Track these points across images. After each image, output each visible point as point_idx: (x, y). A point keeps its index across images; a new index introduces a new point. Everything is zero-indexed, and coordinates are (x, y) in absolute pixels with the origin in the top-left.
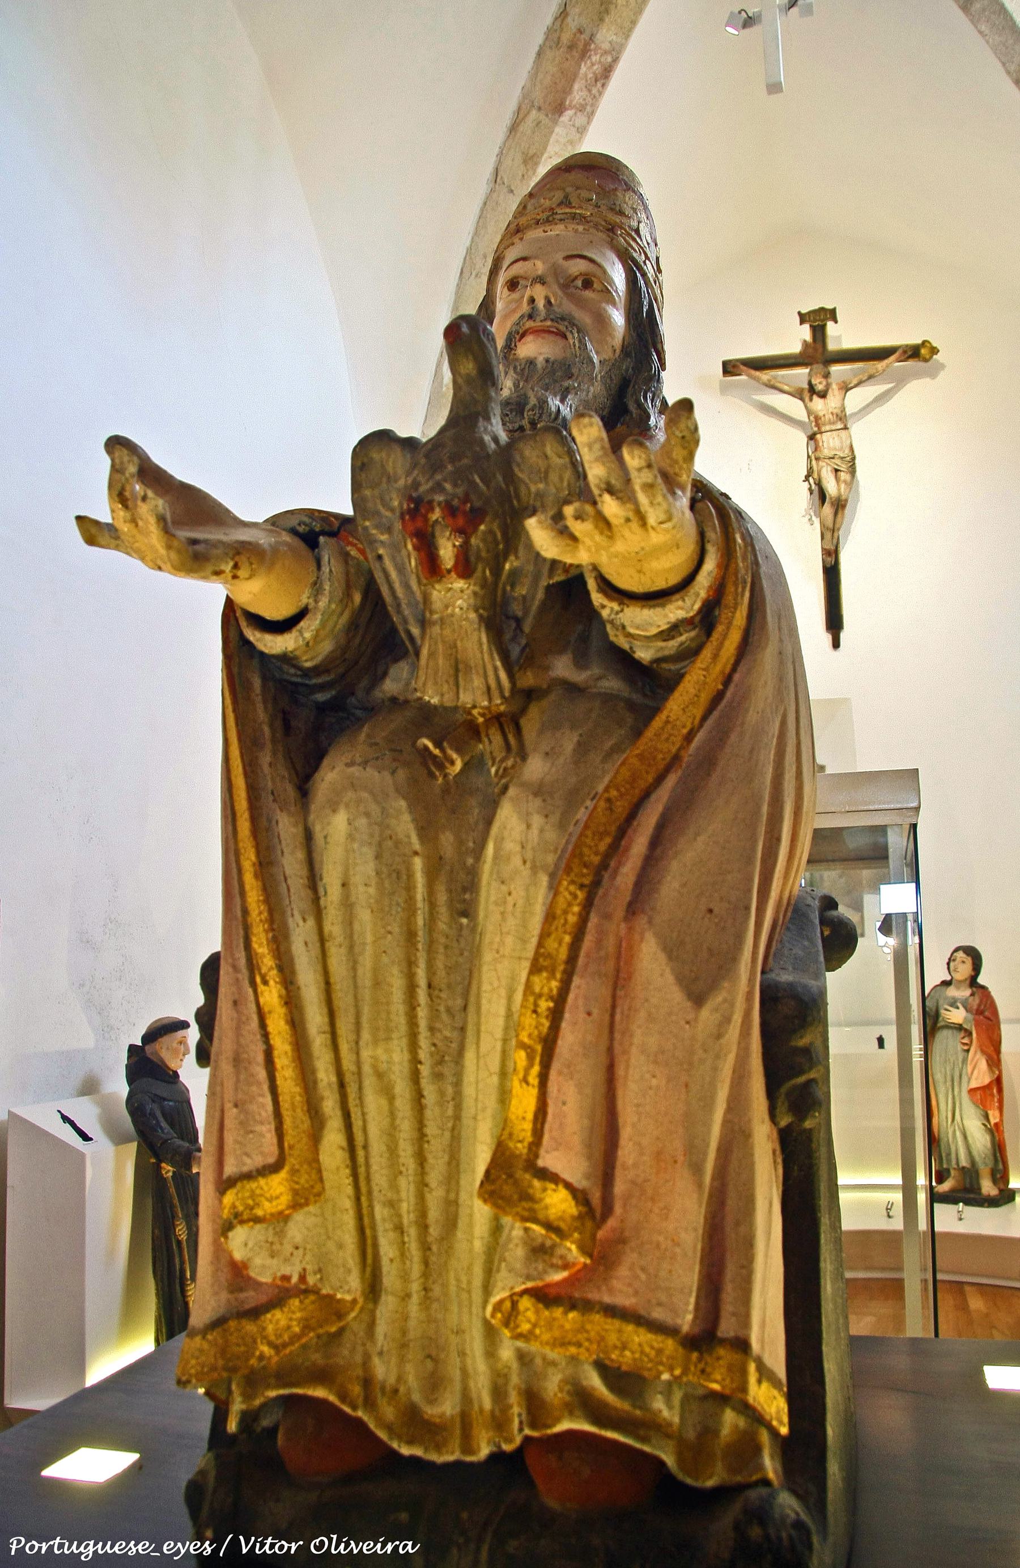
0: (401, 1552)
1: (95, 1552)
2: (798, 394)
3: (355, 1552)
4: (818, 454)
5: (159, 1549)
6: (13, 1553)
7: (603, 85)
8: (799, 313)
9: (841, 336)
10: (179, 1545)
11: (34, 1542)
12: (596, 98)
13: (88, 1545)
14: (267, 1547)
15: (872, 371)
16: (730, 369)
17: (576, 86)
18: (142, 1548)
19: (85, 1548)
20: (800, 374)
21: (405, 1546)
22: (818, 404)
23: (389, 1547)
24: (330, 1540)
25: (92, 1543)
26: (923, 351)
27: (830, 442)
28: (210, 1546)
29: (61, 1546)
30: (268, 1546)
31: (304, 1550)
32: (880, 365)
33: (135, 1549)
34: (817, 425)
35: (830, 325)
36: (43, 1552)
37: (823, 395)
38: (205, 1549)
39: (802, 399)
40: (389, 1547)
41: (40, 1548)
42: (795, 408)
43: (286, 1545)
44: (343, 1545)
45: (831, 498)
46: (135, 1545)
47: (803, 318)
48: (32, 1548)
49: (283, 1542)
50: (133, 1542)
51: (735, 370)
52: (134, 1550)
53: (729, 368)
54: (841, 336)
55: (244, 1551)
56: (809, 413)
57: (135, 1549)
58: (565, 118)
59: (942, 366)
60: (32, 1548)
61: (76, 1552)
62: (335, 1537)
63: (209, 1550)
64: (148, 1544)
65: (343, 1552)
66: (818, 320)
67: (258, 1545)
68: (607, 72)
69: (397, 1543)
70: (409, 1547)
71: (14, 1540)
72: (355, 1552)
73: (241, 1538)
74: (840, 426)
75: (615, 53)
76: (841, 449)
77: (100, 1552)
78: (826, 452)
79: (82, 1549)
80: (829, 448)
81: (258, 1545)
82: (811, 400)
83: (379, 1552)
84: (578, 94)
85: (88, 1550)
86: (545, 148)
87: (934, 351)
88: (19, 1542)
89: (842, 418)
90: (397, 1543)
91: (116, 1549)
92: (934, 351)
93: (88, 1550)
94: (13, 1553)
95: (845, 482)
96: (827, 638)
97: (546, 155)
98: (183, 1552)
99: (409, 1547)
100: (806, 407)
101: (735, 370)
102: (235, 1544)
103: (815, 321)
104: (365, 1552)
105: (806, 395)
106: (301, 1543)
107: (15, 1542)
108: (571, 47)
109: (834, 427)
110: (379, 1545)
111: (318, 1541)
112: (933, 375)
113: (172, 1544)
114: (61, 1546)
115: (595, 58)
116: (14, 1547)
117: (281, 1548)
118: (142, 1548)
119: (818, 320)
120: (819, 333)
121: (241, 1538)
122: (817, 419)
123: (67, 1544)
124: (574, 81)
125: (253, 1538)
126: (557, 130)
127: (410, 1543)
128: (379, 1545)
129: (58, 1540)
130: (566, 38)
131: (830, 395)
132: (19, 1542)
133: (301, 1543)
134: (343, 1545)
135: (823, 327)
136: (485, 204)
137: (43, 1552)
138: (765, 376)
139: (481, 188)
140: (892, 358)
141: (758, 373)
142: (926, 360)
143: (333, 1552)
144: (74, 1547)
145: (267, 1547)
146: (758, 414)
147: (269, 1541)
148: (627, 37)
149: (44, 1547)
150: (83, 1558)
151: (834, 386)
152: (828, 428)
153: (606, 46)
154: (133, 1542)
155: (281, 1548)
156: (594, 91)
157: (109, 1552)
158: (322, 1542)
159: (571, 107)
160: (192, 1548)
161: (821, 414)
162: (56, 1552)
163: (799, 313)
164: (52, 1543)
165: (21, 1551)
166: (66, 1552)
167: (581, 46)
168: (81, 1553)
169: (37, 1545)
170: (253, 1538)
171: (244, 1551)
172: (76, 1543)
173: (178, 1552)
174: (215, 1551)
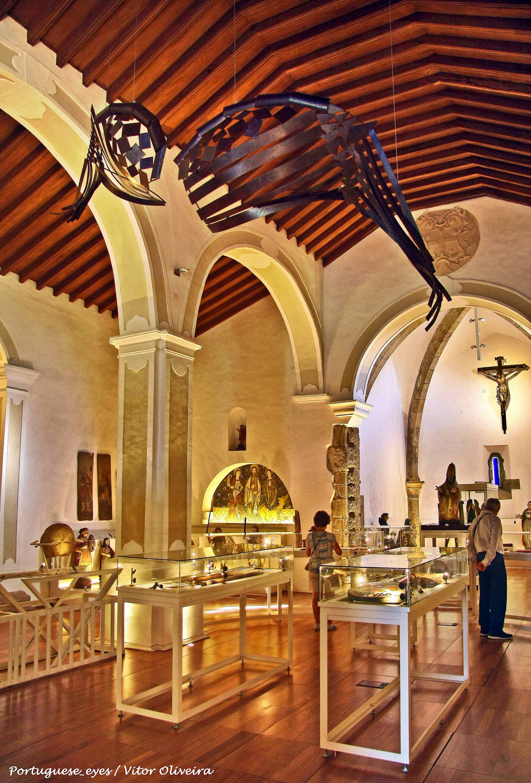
0: (205, 774)
1: (52, 774)
3: (182, 774)
5: (84, 772)
6: (11, 774)
10: (94, 770)
11: (21, 769)
13: (48, 770)
14: (138, 772)
18: (75, 772)
21: (207, 771)
24: (169, 768)
25: (50, 769)
28: (109, 771)
29: (35, 771)
30: (139, 771)
31: (156, 773)
36: (26, 774)
40: (199, 772)
44: (176, 770)
46: (72, 771)
48: (21, 772)
50: (71, 769)
55: (127, 773)
60: (21, 772)
61: (42, 774)
62: (172, 766)
63: (109, 773)
67: (133, 770)
69: (203, 769)
70: (209, 772)
71: (12, 768)
72: (182, 774)
73: (125, 767)
77: (54, 774)
79: (45, 772)
81: (133, 770)
83: (194, 774)
84: (445, 339)
85: (49, 773)
90: (203, 769)
91: (62, 772)
94: (11, 774)
98: (96, 774)
99: (209, 772)
106: (155, 769)
107: (12, 769)
110: (194, 771)
111: (163, 768)
114: (35, 771)
116: (12, 771)
117: (145, 772)
121: (125, 767)
123: (38, 770)
125: (131, 767)
127: (209, 770)
128: (194, 771)
130: (442, 330)
133: (155, 769)
134: (176, 770)
145: (138, 772)
147: (139, 768)
154: (71, 769)
155: (145, 772)
157: (59, 774)
158: (165, 769)
164: (30, 769)
165: (15, 773)
166: (38, 774)
168: (45, 775)
169: (23, 771)
170: (131, 767)
171: (127, 773)
173: (94, 774)
174: (112, 774)
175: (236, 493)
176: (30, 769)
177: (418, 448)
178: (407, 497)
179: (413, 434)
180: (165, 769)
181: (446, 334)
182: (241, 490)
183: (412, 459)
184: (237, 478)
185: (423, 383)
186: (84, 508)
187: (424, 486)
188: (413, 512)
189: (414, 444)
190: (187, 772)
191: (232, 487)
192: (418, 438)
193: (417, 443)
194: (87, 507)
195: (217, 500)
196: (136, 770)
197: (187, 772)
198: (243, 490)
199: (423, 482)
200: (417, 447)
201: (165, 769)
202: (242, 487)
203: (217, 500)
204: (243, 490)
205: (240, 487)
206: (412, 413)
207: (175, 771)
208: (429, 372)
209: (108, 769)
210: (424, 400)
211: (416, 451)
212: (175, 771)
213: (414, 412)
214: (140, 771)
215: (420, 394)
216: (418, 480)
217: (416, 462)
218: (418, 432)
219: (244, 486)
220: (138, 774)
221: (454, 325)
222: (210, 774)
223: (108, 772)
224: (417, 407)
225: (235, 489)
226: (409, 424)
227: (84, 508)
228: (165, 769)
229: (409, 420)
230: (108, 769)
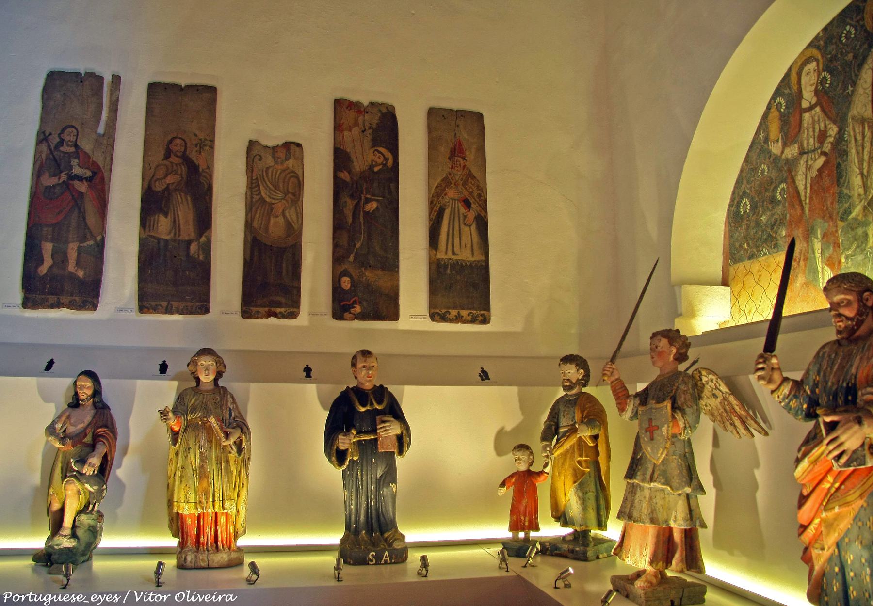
5: (88, 599)
23: (220, 598)
29: (33, 597)
40: (220, 598)
91: (64, 599)
114: (33, 597)
116: (6, 598)
129: (31, 594)
132: (9, 595)
138: (597, 479)
147: (151, 594)
158: (181, 595)
165: (10, 600)
174: (121, 600)
175: (808, 168)
180: (181, 595)
182: (827, 147)
184: (808, 97)
186: (48, 262)
191: (792, 151)
194: (65, 260)
195: (741, 232)
196: (148, 597)
198: (840, 138)
202: (833, 130)
203: (741, 232)
204: (840, 138)
205: (822, 136)
207: (193, 597)
212: (193, 597)
214: (153, 597)
219: (841, 121)
225: (802, 152)
227: (48, 262)
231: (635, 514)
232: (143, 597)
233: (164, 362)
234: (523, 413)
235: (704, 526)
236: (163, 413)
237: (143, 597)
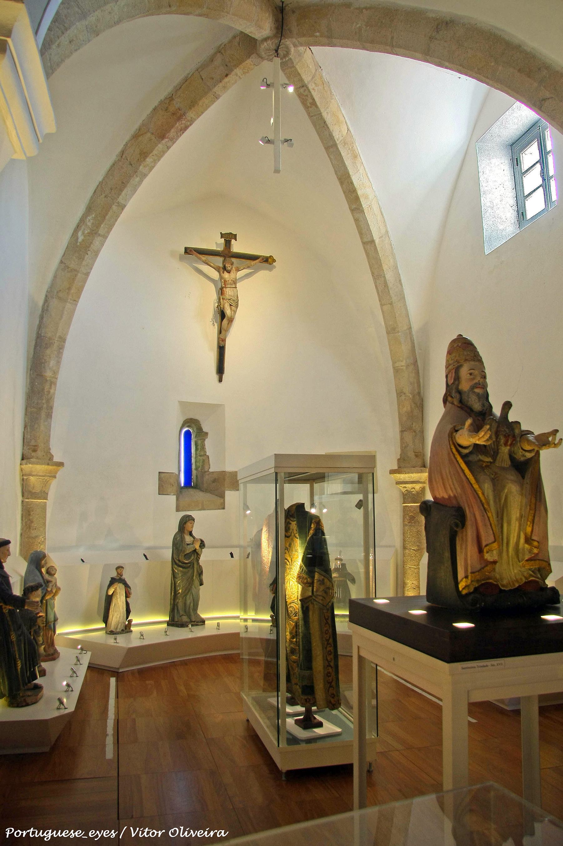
0: (218, 836)
1: (52, 836)
2: (217, 269)
3: (193, 836)
4: (224, 297)
6: (7, 837)
7: (183, 133)
8: (221, 233)
9: (237, 247)
10: (98, 832)
11: (19, 831)
12: (178, 137)
13: (48, 832)
14: (145, 833)
15: (249, 265)
16: (188, 251)
17: (173, 130)
18: (77, 834)
19: (47, 834)
20: (219, 261)
21: (221, 832)
22: (226, 275)
23: (212, 833)
24: (180, 830)
25: (50, 831)
26: (269, 260)
27: (229, 292)
28: (115, 833)
29: (34, 833)
30: (146, 833)
31: (165, 835)
32: (253, 263)
33: (73, 834)
34: (225, 284)
35: (233, 241)
36: (24, 836)
37: (229, 272)
38: (112, 834)
39: (219, 272)
40: (212, 833)
41: (22, 834)
42: (215, 275)
43: (156, 832)
44: (186, 832)
45: (228, 317)
46: (74, 832)
47: (222, 235)
48: (18, 834)
49: (154, 831)
50: (73, 831)
51: (191, 253)
52: (73, 835)
53: (188, 251)
54: (237, 247)
55: (133, 835)
56: (221, 277)
57: (73, 834)
58: (164, 142)
59: (275, 267)
60: (18, 834)
61: (42, 836)
62: (182, 828)
63: (114, 835)
64: (81, 832)
65: (186, 836)
66: (229, 238)
67: (140, 832)
68: (186, 128)
69: (216, 831)
70: (223, 833)
71: (8, 830)
72: (193, 836)
73: (131, 828)
74: (234, 286)
75: (192, 122)
76: (234, 296)
77: (55, 836)
78: (227, 297)
79: (45, 834)
80: (229, 295)
81: (140, 832)
82: (223, 273)
83: (206, 836)
84: (172, 133)
85: (48, 835)
86: (152, 151)
87: (274, 261)
88: (11, 831)
89: (235, 282)
90: (216, 831)
91: (63, 834)
92: (274, 261)
93: (48, 835)
94: (7, 837)
95: (234, 311)
96: (216, 377)
97: (151, 154)
98: (100, 836)
99: (223, 833)
100: (220, 275)
101: (191, 253)
102: (128, 832)
103: (227, 238)
104: (105, 836)
105: (222, 271)
106: (164, 831)
107: (9, 831)
108: (174, 114)
109: (231, 286)
110: (206, 832)
111: (173, 830)
112: (270, 270)
113: (94, 832)
114: (34, 833)
115: (183, 122)
116: (8, 833)
117: (153, 834)
118: (77, 834)
119: (229, 238)
120: (228, 243)
121: (131, 828)
122: (225, 281)
123: (37, 832)
124: (172, 128)
125: (138, 829)
126: (159, 145)
127: (223, 831)
128: (206, 832)
129: (32, 830)
130: (172, 109)
131: (232, 273)
132: (11, 831)
133: (164, 831)
134: (186, 832)
135: (230, 241)
136: (114, 164)
137: (24, 836)
138: (204, 258)
139: (113, 158)
140: (257, 261)
141: (200, 256)
142: (270, 264)
143: (181, 836)
144: (59, 833)
145: (145, 833)
146: (195, 272)
147: (147, 830)
148: (198, 117)
149: (25, 833)
150: (45, 839)
151: (234, 269)
152: (229, 286)
153: (189, 118)
154: (73, 831)
155: (153, 834)
156: (179, 134)
157: (60, 836)
158: (175, 831)
159: (167, 138)
160: (198, 834)
161: (227, 280)
162: (31, 836)
163: (221, 233)
164: (28, 831)
165: (12, 835)
166: (36, 836)
167: (178, 115)
168: (44, 837)
169: (20, 832)
170: (138, 829)
171: (133, 835)
172: (41, 831)
173: (97, 836)
176: (28, 831)
177: (55, 384)
178: (20, 498)
179: (48, 352)
180: (175, 831)
181: (179, 119)
183: (40, 409)
185: (94, 233)
187: (61, 472)
188: (34, 533)
189: (48, 374)
190: (199, 834)
192: (59, 363)
193: (55, 373)
197: (199, 834)
199: (61, 464)
200: (53, 383)
201: (175, 830)
206: (54, 303)
208: (114, 207)
209: (113, 831)
210: (87, 274)
211: (52, 391)
213: (60, 298)
215: (81, 259)
216: (49, 459)
217: (49, 415)
218: (61, 348)
220: (146, 836)
221: (205, 101)
222: (223, 836)
223: (113, 834)
224: (69, 289)
226: (40, 327)
228: (175, 830)
229: (42, 318)
230: (113, 831)
231: (25, 461)
232: (138, 832)
233: (179, 401)
234: (512, 422)
235: (353, 581)
236: (202, 545)
237: (138, 832)
